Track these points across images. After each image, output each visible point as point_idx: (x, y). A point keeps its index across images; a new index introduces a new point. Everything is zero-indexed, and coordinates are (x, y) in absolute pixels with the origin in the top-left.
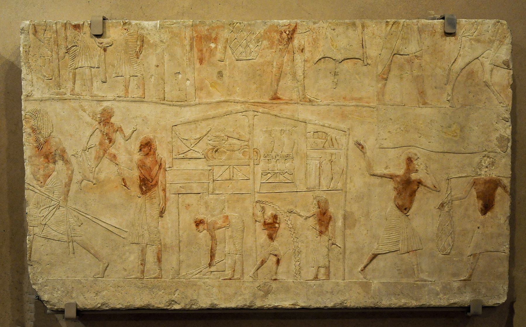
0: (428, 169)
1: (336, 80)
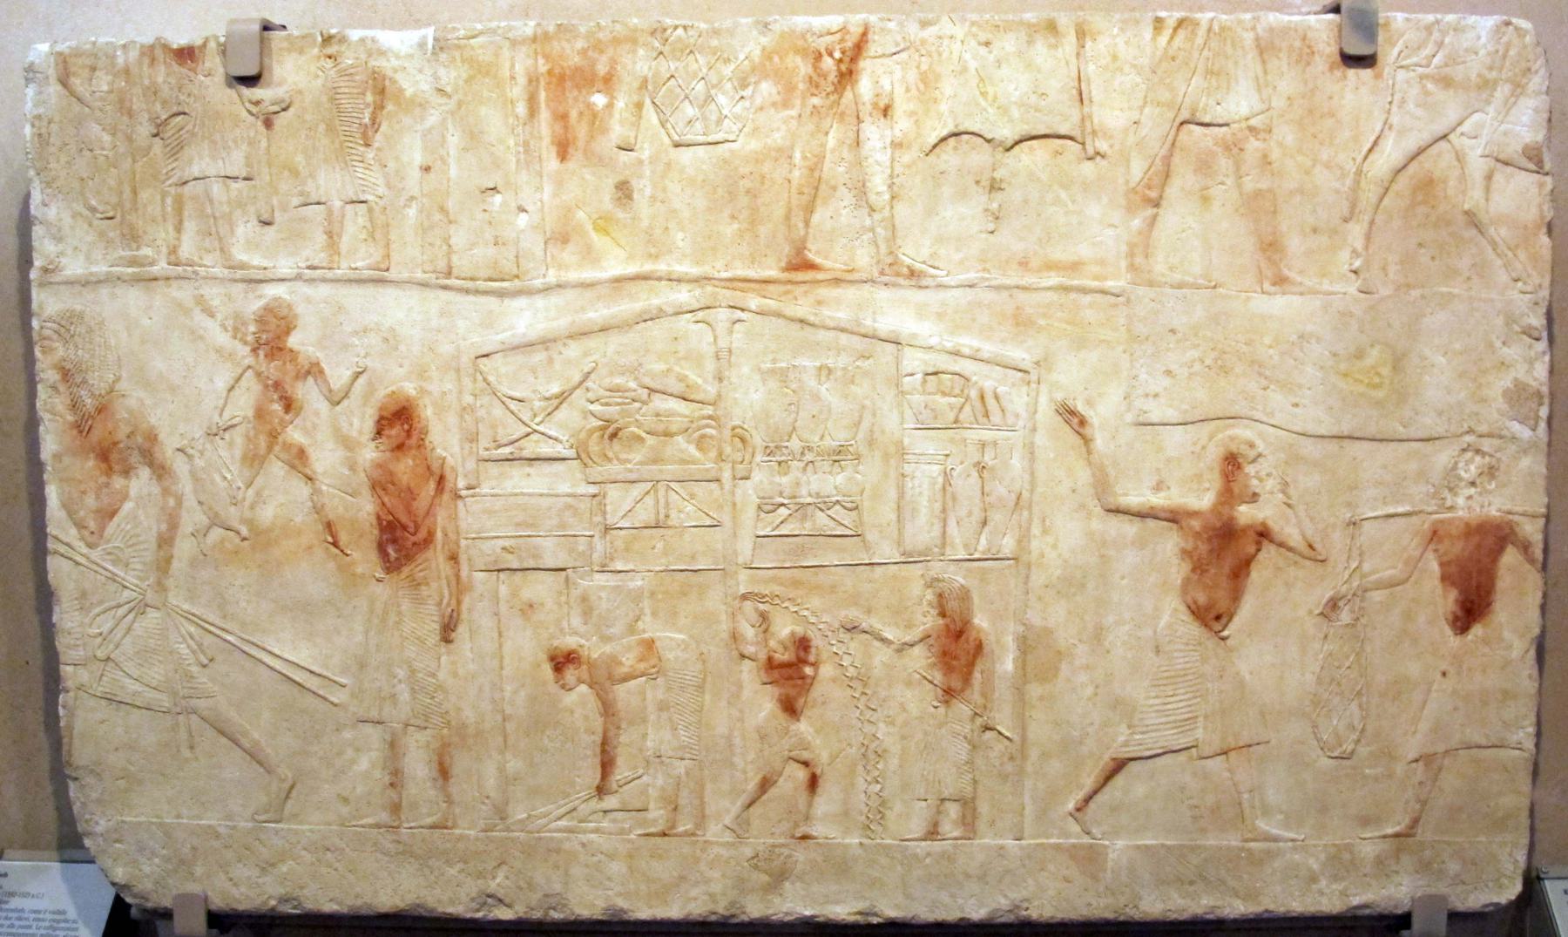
0: (1292, 491)
1: (995, 205)
